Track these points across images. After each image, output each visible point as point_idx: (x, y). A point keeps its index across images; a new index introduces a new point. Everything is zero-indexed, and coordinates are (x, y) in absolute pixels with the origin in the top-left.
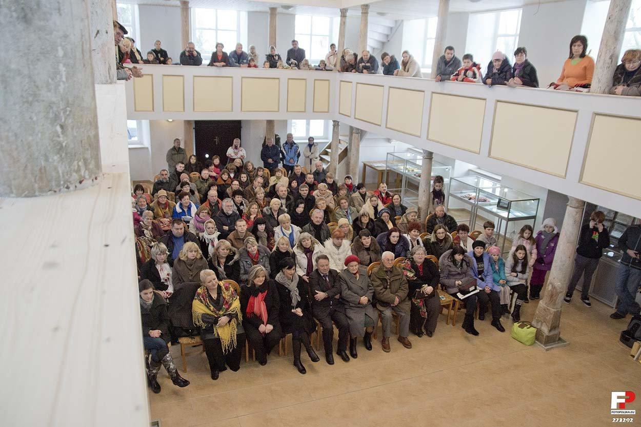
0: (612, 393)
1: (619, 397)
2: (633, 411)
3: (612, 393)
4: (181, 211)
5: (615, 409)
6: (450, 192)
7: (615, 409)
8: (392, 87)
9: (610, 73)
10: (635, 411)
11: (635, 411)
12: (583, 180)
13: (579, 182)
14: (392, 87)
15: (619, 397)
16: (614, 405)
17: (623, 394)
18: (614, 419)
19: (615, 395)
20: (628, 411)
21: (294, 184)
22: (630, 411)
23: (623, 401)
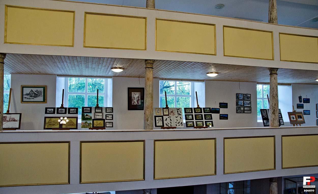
0: (304, 177)
1: (307, 179)
2: (314, 186)
3: (304, 177)
4: (264, 121)
5: (305, 185)
6: (144, 49)
7: (305, 185)
8: (212, 55)
9: (303, 82)
10: (315, 186)
11: (315, 186)
12: (82, 181)
13: (80, 184)
14: (212, 55)
15: (307, 179)
16: (304, 183)
17: (309, 178)
18: (305, 190)
19: (305, 178)
20: (312, 186)
21: (265, 121)
22: (313, 186)
23: (309, 181)
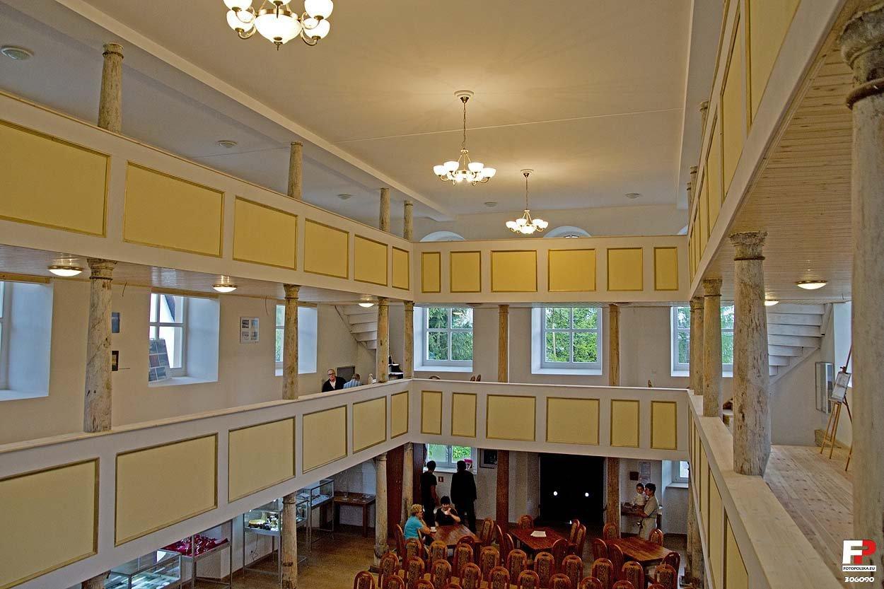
16: (847, 559)
17: (859, 543)
23: (859, 553)
